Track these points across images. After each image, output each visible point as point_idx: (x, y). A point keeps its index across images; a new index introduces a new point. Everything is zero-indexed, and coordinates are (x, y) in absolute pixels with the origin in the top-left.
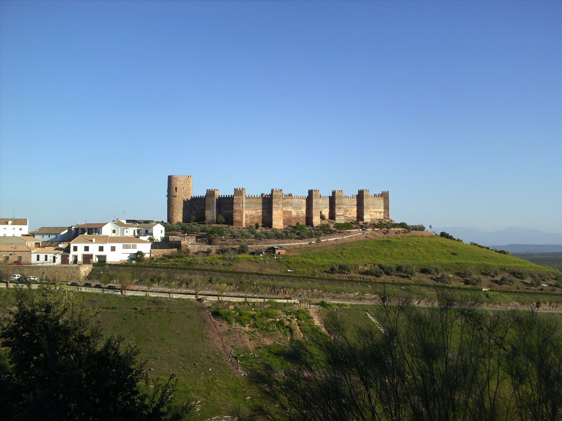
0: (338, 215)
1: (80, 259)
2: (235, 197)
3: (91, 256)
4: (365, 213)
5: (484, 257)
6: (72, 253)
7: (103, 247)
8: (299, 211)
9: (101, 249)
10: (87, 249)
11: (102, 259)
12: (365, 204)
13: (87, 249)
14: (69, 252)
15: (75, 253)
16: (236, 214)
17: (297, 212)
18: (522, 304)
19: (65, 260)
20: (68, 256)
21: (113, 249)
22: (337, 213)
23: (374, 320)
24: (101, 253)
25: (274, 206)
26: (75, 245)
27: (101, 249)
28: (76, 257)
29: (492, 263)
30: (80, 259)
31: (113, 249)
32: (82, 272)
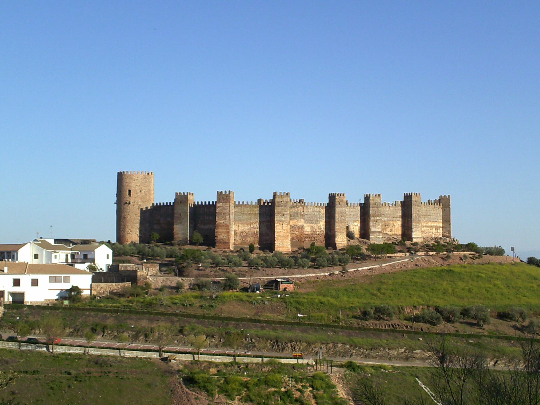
0: (374, 232)
2: (218, 205)
8: (315, 226)
9: (17, 283)
17: (312, 228)
21: (35, 283)
22: (372, 229)
24: (17, 289)
27: (17, 283)
31: (35, 283)
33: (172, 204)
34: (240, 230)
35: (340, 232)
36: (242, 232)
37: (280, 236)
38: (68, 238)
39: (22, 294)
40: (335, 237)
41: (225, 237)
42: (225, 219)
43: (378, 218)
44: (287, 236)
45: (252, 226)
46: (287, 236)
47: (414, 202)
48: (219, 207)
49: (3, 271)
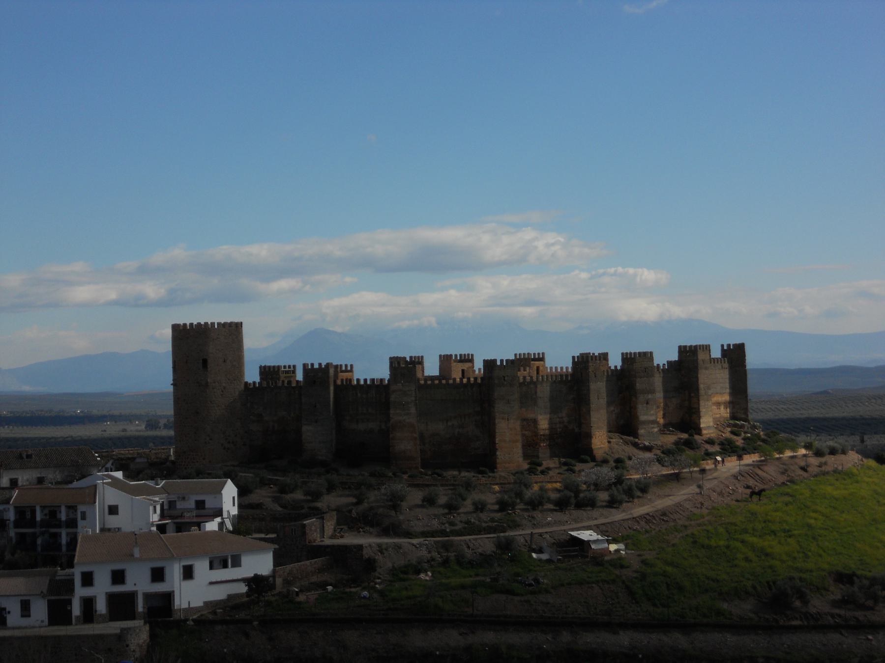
0: (644, 423)
1: (101, 606)
2: (393, 388)
4: (703, 410)
5: (737, 501)
6: (80, 592)
7: (22, 616)
10: (118, 577)
12: (701, 386)
13: (118, 577)
14: (71, 589)
15: (87, 592)
19: (59, 613)
20: (70, 602)
21: (188, 573)
22: (643, 418)
25: (499, 407)
27: (158, 575)
28: (88, 604)
30: (101, 606)
32: (132, 647)
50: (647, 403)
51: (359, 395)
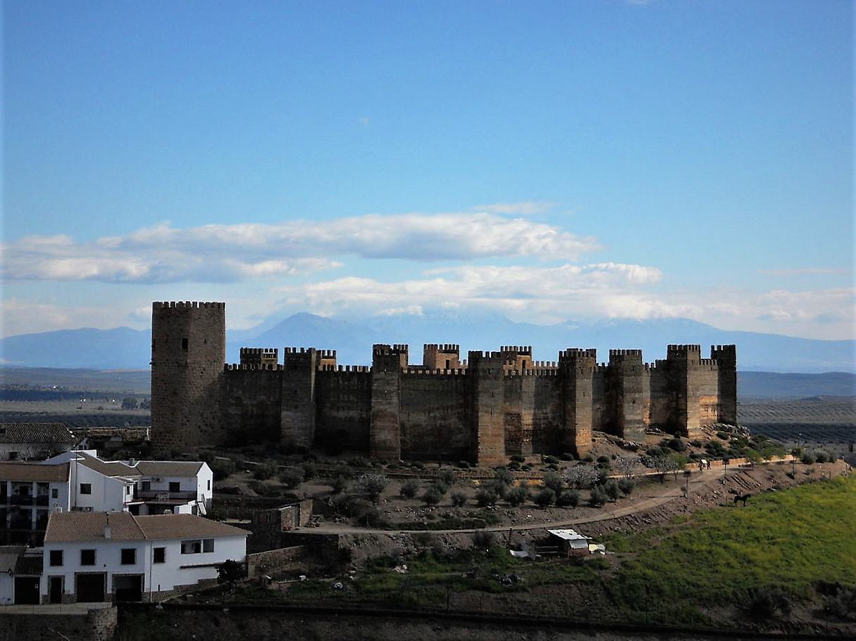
0: (630, 422)
1: (69, 587)
2: (376, 376)
3: (101, 577)
4: (690, 411)
6: (49, 571)
10: (88, 557)
11: (131, 587)
13: (88, 557)
16: (378, 424)
18: (823, 497)
20: (37, 581)
21: (159, 556)
22: (628, 417)
23: (34, 520)
24: (130, 570)
26: (56, 548)
28: (56, 582)
29: (797, 399)
30: (69, 587)
33: (464, 373)
34: (411, 423)
35: (582, 425)
36: (416, 426)
37: (487, 435)
38: (46, 366)
39: (138, 580)
40: (575, 435)
41: (389, 437)
42: (389, 403)
43: (637, 396)
44: (499, 435)
45: (432, 415)
46: (499, 435)
47: (689, 362)
48: (377, 380)
49: (103, 536)
50: (634, 403)
51: (341, 382)
